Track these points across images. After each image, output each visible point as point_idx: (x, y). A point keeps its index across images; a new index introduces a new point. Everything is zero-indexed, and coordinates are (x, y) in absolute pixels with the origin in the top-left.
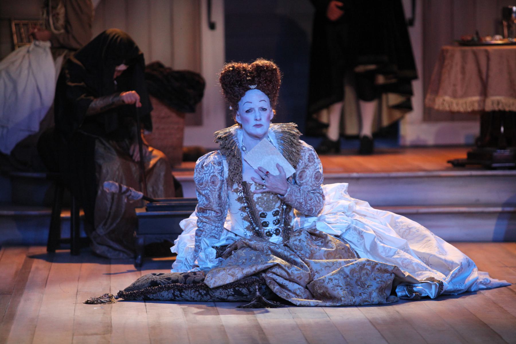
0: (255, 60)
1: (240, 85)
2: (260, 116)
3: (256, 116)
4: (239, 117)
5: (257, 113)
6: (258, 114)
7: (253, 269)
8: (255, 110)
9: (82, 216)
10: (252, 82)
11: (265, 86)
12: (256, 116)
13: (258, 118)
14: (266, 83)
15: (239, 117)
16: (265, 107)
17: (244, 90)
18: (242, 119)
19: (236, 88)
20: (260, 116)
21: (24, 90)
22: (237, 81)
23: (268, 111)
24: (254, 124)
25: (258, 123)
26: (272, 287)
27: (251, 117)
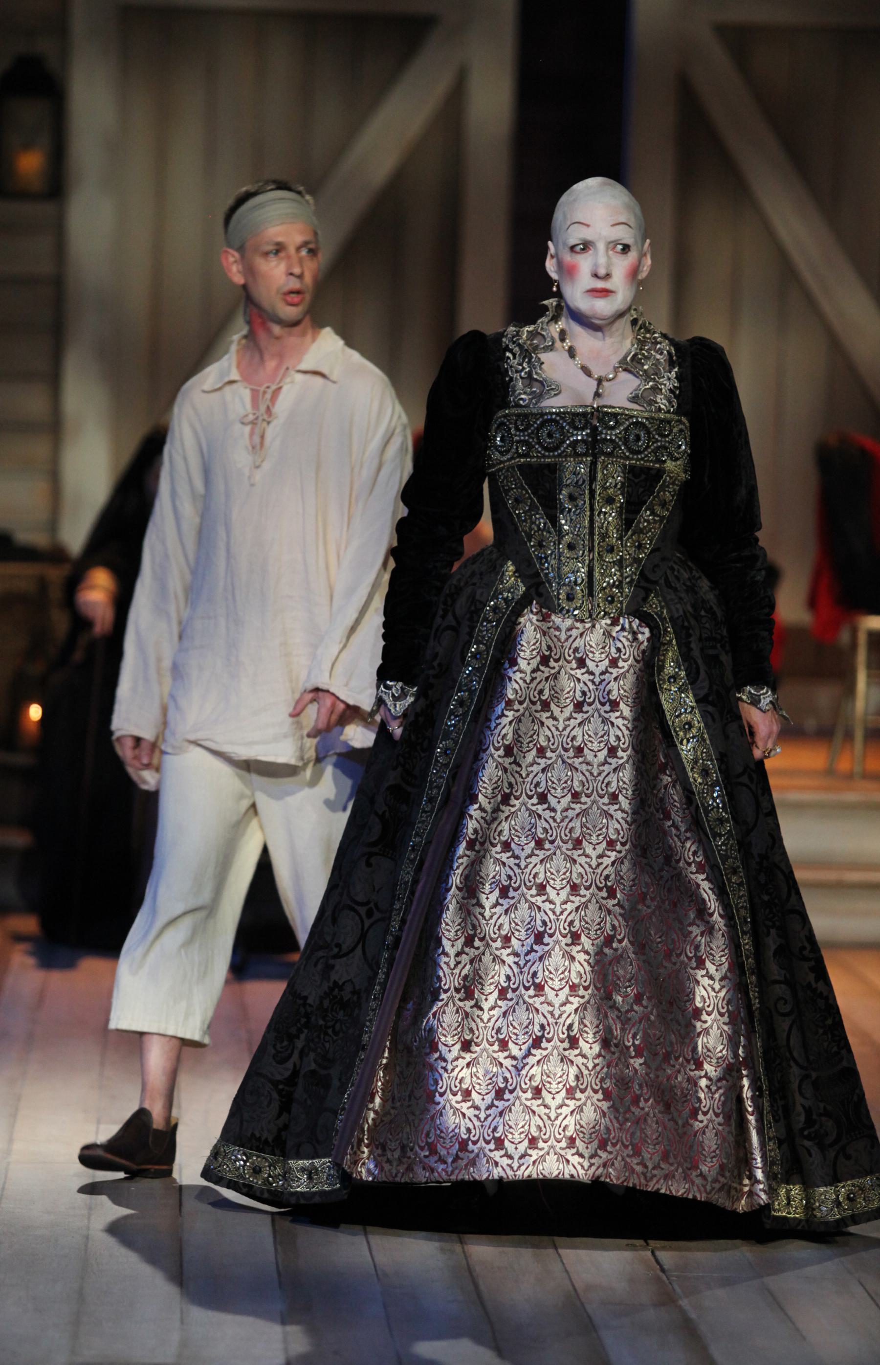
0: (329, 1191)
2: (609, 265)
3: (596, 265)
4: (554, 260)
5: (600, 257)
6: (602, 260)
7: (587, 492)
8: (596, 249)
9: (27, 146)
12: (596, 265)
13: (602, 272)
15: (554, 260)
16: (629, 241)
20: (609, 265)
21: (297, 877)
23: (633, 255)
24: (589, 287)
25: (600, 284)
26: (743, 902)
27: (585, 264)
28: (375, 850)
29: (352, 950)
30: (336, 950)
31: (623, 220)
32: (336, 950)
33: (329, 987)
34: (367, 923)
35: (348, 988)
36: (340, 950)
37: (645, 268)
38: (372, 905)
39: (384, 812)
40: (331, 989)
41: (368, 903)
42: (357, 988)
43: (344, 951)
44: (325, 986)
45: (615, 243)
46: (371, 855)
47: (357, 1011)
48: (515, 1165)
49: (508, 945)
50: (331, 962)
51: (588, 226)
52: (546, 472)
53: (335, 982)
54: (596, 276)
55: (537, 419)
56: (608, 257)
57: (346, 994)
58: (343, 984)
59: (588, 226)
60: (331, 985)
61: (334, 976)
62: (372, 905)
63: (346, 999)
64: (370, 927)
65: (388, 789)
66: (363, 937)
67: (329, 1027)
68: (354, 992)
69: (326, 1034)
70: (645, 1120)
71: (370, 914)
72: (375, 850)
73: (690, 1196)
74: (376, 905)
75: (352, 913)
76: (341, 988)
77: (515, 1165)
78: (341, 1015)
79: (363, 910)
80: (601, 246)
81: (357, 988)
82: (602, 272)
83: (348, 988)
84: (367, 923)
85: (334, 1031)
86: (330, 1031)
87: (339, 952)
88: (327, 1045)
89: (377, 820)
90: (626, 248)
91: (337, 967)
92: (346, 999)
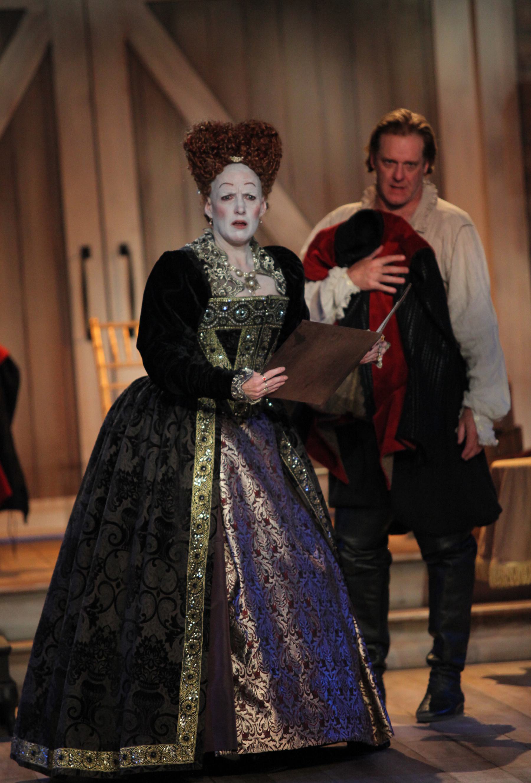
1: (217, 155)
2: (244, 207)
3: (237, 207)
4: (211, 207)
8: (236, 197)
10: (236, 153)
11: (256, 161)
12: (237, 207)
13: (241, 210)
14: (258, 155)
17: (221, 163)
18: (215, 210)
19: (209, 160)
20: (244, 207)
22: (213, 148)
25: (240, 218)
28: (157, 556)
29: (151, 618)
30: (143, 618)
31: (250, 181)
32: (143, 618)
33: (142, 640)
34: (117, 591)
35: (107, 631)
36: (146, 617)
37: (263, 211)
38: (120, 580)
39: (157, 533)
40: (143, 641)
41: (117, 579)
42: (112, 630)
43: (148, 618)
44: (94, 629)
45: (247, 195)
46: (154, 559)
47: (113, 645)
48: (278, 745)
49: (246, 616)
50: (141, 625)
51: (232, 185)
52: (234, 334)
53: (145, 637)
54: (237, 213)
55: (236, 304)
56: (244, 203)
57: (106, 634)
58: (104, 627)
59: (232, 185)
60: (143, 638)
61: (144, 633)
62: (120, 580)
63: (153, 646)
64: (119, 593)
65: (156, 519)
66: (115, 600)
67: (146, 664)
68: (111, 633)
69: (144, 668)
70: (304, 708)
71: (118, 585)
72: (157, 556)
73: (307, 746)
74: (122, 580)
75: (149, 595)
76: (149, 640)
77: (278, 745)
78: (102, 646)
79: (114, 584)
80: (240, 197)
81: (112, 630)
82: (241, 210)
83: (107, 631)
84: (117, 591)
85: (149, 667)
86: (146, 667)
87: (144, 619)
88: (146, 675)
89: (153, 538)
90: (252, 198)
91: (145, 628)
92: (153, 646)
